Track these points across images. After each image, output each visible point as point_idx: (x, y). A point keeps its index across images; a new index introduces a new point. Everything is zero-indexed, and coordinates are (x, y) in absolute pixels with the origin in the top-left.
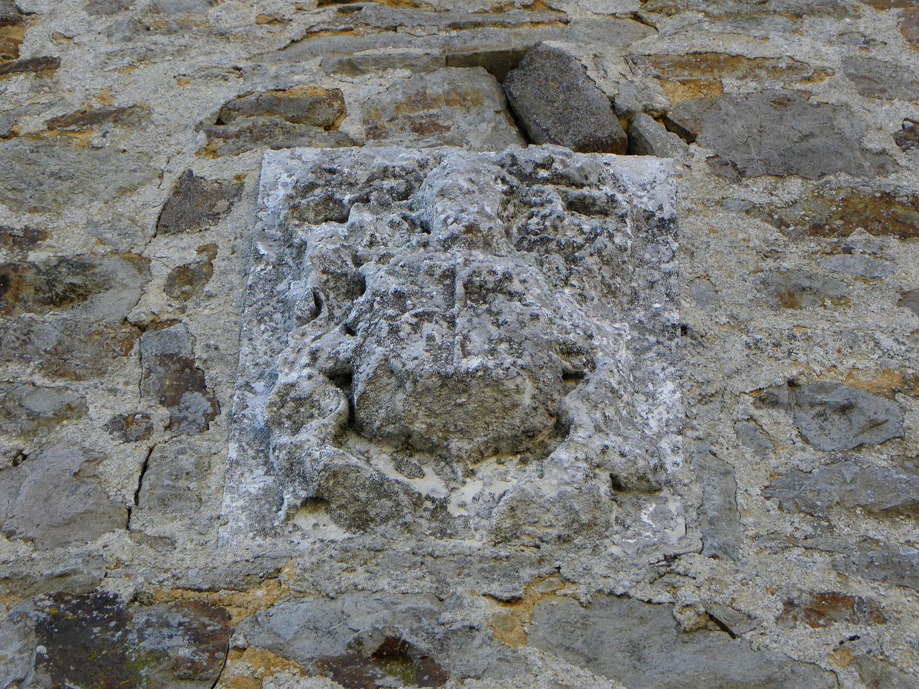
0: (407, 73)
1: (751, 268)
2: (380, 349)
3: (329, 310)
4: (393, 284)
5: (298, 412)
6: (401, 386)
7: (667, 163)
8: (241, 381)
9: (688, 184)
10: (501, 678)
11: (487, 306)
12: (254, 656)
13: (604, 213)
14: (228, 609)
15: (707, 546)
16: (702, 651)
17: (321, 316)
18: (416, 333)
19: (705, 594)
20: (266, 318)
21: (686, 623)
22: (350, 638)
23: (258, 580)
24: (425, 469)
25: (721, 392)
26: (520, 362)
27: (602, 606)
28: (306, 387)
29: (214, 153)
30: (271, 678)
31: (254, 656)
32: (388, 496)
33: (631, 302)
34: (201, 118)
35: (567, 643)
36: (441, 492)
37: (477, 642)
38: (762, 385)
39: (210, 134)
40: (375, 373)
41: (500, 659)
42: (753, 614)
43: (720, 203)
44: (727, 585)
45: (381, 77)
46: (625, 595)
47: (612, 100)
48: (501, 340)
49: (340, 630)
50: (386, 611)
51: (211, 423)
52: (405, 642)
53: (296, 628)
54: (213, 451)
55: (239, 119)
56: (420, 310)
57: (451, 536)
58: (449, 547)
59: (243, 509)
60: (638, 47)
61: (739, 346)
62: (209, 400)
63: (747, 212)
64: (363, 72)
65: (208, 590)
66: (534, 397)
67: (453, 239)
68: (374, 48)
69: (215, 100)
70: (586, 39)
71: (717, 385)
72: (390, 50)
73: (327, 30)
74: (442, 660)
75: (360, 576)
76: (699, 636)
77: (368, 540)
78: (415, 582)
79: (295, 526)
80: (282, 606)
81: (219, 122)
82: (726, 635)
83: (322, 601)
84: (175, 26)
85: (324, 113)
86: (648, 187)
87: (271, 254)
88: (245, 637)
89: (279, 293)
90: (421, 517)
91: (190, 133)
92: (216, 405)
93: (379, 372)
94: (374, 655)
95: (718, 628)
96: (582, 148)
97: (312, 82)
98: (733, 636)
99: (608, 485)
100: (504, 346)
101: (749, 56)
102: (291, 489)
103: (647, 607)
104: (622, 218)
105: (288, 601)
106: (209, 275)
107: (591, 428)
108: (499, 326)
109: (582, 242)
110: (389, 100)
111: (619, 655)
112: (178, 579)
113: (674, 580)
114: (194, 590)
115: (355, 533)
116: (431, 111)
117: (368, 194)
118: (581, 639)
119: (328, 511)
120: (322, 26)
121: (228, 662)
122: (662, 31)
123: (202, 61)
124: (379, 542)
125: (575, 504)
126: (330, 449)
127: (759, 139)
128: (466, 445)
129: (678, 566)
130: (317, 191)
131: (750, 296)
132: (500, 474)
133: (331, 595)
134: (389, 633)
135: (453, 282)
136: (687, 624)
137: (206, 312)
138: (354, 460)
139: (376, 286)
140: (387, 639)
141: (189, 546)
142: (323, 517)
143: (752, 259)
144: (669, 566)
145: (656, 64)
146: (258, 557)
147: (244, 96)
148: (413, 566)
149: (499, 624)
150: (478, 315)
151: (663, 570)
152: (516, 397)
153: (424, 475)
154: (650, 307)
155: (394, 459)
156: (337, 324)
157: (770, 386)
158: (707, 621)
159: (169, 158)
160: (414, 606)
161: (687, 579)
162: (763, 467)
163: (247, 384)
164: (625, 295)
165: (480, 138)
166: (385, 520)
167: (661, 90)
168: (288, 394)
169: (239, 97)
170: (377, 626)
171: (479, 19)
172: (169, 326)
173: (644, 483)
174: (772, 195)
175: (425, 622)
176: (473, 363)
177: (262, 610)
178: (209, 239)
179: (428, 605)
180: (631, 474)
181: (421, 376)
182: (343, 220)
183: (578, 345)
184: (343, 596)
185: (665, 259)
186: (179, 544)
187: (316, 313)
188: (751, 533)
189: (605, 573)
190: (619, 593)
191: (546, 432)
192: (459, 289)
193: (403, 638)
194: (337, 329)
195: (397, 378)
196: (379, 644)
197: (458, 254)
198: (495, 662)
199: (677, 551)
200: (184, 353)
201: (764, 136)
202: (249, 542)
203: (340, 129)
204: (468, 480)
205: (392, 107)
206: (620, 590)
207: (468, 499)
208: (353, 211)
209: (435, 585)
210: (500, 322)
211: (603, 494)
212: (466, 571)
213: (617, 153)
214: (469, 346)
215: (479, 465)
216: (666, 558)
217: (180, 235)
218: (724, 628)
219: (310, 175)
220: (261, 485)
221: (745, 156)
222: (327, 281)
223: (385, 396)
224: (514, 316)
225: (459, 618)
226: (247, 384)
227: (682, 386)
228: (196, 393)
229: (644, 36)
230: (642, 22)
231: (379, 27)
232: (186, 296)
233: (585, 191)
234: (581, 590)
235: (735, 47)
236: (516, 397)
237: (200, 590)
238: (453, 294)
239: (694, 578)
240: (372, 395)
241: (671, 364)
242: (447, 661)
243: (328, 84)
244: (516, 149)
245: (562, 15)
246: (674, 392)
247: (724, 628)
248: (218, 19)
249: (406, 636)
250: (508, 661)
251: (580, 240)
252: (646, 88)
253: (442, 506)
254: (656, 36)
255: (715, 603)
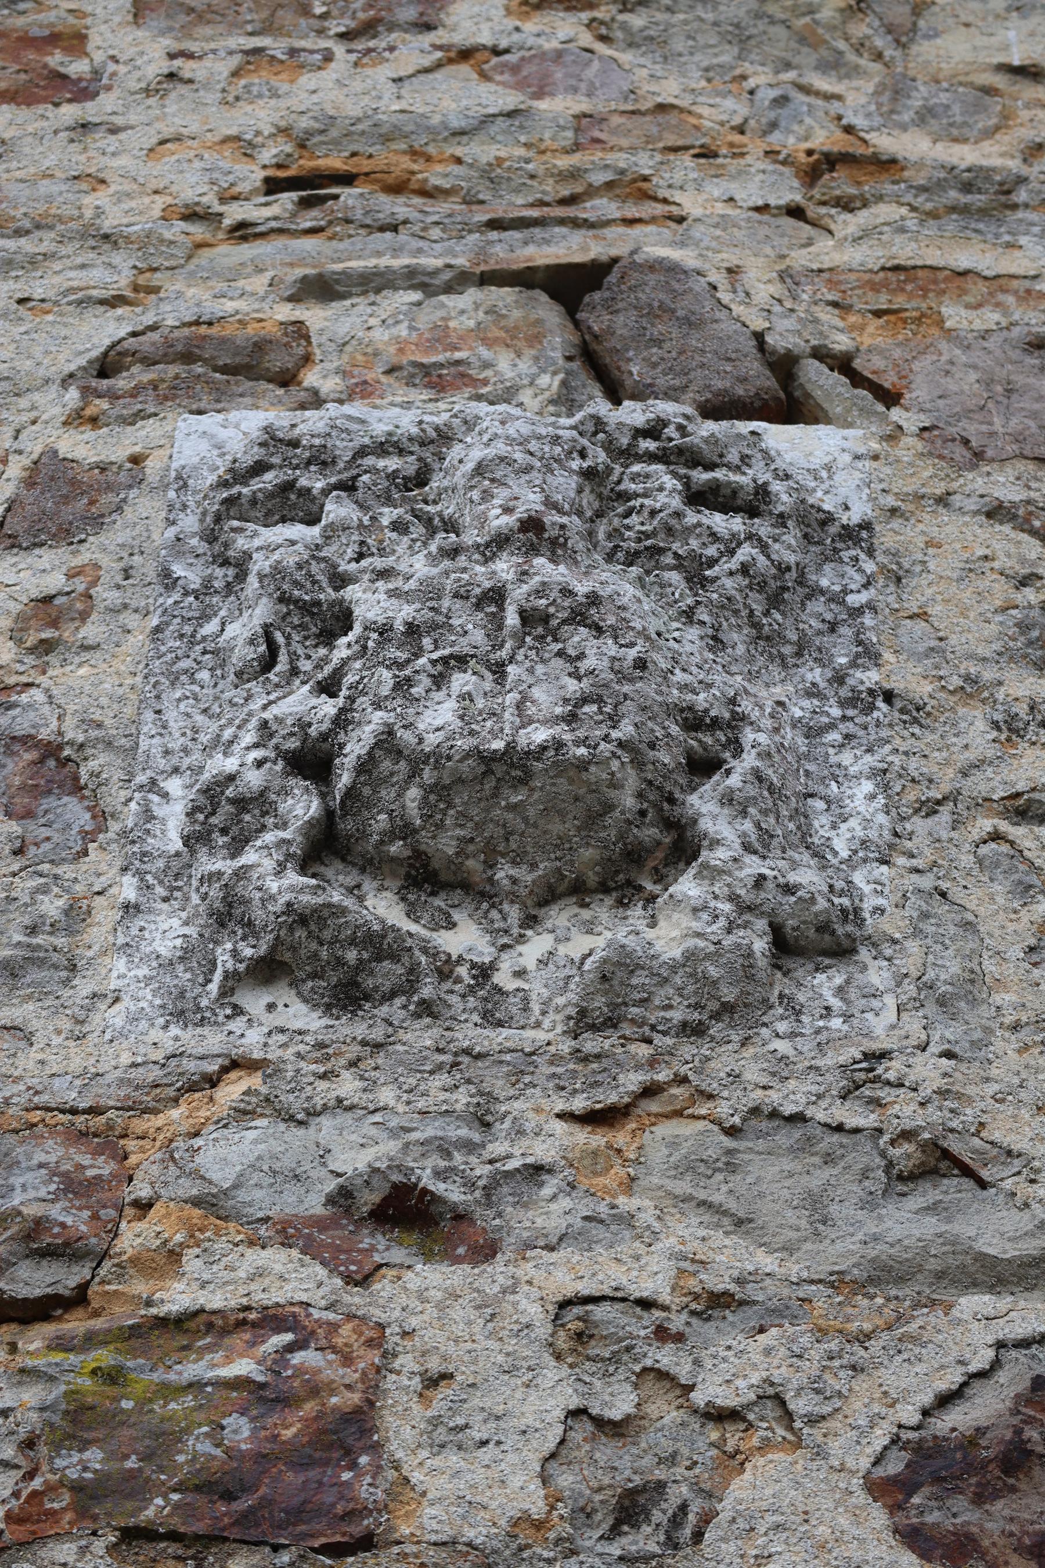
0: (416, 296)
1: (998, 603)
2: (380, 714)
3: (291, 662)
4: (404, 613)
5: (240, 821)
6: (414, 773)
7: (855, 438)
8: (141, 778)
9: (888, 470)
10: (590, 1250)
11: (560, 646)
12: (168, 1215)
13: (752, 512)
14: (122, 1142)
15: (936, 1037)
16: (932, 1209)
17: (278, 668)
18: (439, 689)
19: (934, 1114)
20: (183, 678)
21: (903, 1163)
22: (331, 1185)
23: (173, 1094)
24: (456, 916)
25: (952, 797)
26: (615, 734)
27: (760, 1135)
28: (254, 779)
29: (94, 421)
30: (197, 1251)
31: (168, 1215)
32: (395, 958)
33: (799, 654)
34: (72, 367)
35: (702, 1195)
36: (485, 953)
37: (547, 1191)
38: (1021, 787)
39: (86, 392)
40: (369, 754)
41: (586, 1218)
42: (1015, 1147)
43: (943, 500)
44: (970, 1100)
45: (373, 304)
46: (798, 1118)
47: (759, 337)
48: (585, 700)
49: (314, 1174)
50: (392, 1143)
51: (91, 846)
52: (425, 1191)
53: (238, 1168)
54: (96, 889)
55: (135, 369)
56: (446, 652)
57: (500, 1024)
58: (500, 1039)
59: (148, 980)
60: (800, 259)
61: (981, 725)
62: (89, 809)
63: (989, 515)
64: (343, 297)
65: (85, 1112)
66: (640, 795)
67: (500, 542)
68: (360, 257)
69: (95, 340)
70: (714, 244)
71: (946, 788)
72: (385, 261)
73: (281, 231)
74: (485, 1219)
75: (348, 1086)
76: (925, 1185)
77: (360, 1030)
78: (443, 1096)
79: (235, 1007)
80: (214, 1135)
81: (103, 374)
82: (968, 1183)
83: (282, 1126)
84: (27, 224)
85: (277, 361)
86: (824, 474)
87: (191, 576)
88: (152, 1184)
89: (204, 639)
90: (452, 992)
91: (54, 389)
92: (101, 817)
93: (378, 753)
94: (372, 1214)
95: (956, 1172)
96: (711, 411)
97: (257, 311)
98: (983, 1184)
99: (766, 939)
100: (590, 709)
101: (986, 273)
102: (229, 946)
103: (836, 1138)
104: (782, 520)
105: (225, 1126)
106: (84, 616)
107: (737, 846)
108: (579, 679)
109: (716, 554)
110: (386, 338)
111: (789, 1213)
112: (37, 1093)
113: (880, 1094)
114: (63, 1112)
115: (338, 1018)
116: (458, 355)
117: (354, 478)
118: (724, 1188)
119: (294, 984)
120: (274, 224)
121: (123, 1225)
122: (839, 235)
123: (77, 278)
124: (378, 1034)
125: (711, 968)
126: (293, 878)
127: (1005, 401)
128: (526, 877)
129: (887, 1069)
130: (269, 476)
131: (997, 646)
132: (584, 923)
133: (299, 1117)
134: (396, 1177)
135: (502, 609)
136: (904, 1166)
137: (82, 671)
138: (336, 897)
139: (371, 615)
140: (395, 1186)
141: (57, 1040)
142: (282, 993)
143: (1001, 591)
144: (872, 1070)
145: (832, 284)
146: (174, 1056)
147: (142, 333)
148: (439, 1068)
149: (585, 1162)
150: (543, 661)
151: (862, 1076)
152: (613, 794)
153: (455, 925)
154: (831, 662)
155: (403, 899)
156: (304, 683)
157: (1033, 789)
158: (938, 1160)
159: (18, 431)
160: (440, 1133)
161: (903, 1090)
162: (1025, 916)
163: (153, 782)
164: (789, 642)
165: (540, 398)
166: (389, 997)
167: (841, 324)
168: (222, 793)
169: (134, 334)
170: (378, 1165)
171: (535, 213)
172: (19, 693)
173: (827, 937)
174: (1029, 488)
175: (458, 1158)
176: (540, 735)
177: (180, 1144)
178: (85, 556)
179: (464, 1132)
180: (804, 922)
181: (449, 758)
182: (312, 520)
183: (713, 713)
184: (318, 1120)
185: (853, 587)
186: (39, 1040)
187: (268, 663)
188: (1008, 1020)
189: (764, 1080)
190: (787, 1113)
191: (660, 855)
192: (512, 619)
193: (421, 1185)
194: (307, 687)
195: (409, 761)
196: (381, 1196)
197: (504, 567)
198: (579, 1223)
199: (886, 1045)
200: (44, 734)
201: (1015, 397)
202: (155, 1035)
203: (305, 384)
204: (529, 933)
205: (392, 349)
206: (788, 1109)
207: (530, 964)
208: (329, 507)
209: (475, 1100)
210: (582, 671)
211: (758, 954)
212: (527, 1079)
213: (770, 421)
214: (531, 710)
215: (543, 911)
216: (867, 1056)
217: (37, 551)
218: (967, 1172)
219: (256, 449)
220: (179, 942)
221: (984, 428)
222: (288, 614)
223: (387, 794)
224: (606, 663)
225: (517, 1152)
226: (153, 782)
227: (887, 787)
228: (66, 799)
229: (810, 242)
230: (807, 222)
231: (367, 226)
232: (46, 647)
233: (719, 474)
234: (723, 1109)
235: (963, 260)
236: (613, 794)
237: (74, 1111)
238: (500, 627)
239: (915, 1090)
240: (367, 791)
241: (868, 751)
242: (497, 1222)
243: (285, 312)
244: (601, 406)
245: (673, 209)
246: (872, 797)
247: (967, 1172)
248: (99, 211)
249: (427, 1180)
250: (602, 1222)
251: (711, 551)
252: (816, 321)
253: (484, 972)
254: (831, 243)
255: (952, 1130)
